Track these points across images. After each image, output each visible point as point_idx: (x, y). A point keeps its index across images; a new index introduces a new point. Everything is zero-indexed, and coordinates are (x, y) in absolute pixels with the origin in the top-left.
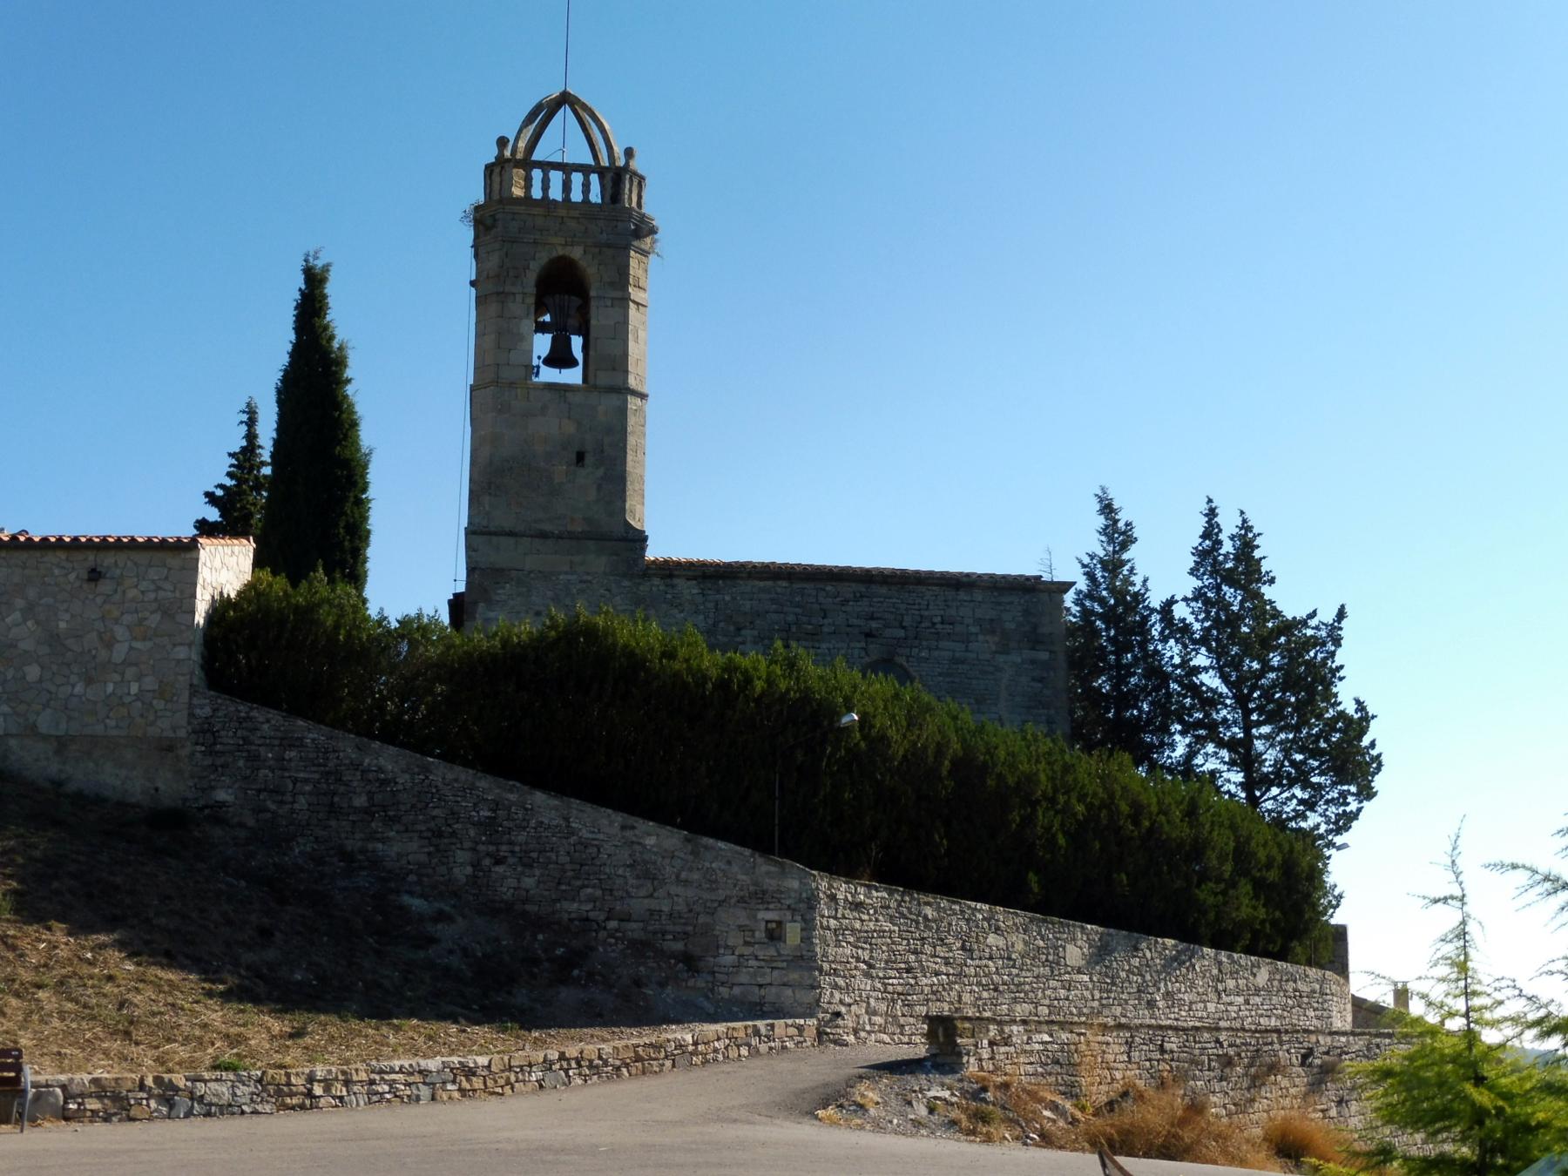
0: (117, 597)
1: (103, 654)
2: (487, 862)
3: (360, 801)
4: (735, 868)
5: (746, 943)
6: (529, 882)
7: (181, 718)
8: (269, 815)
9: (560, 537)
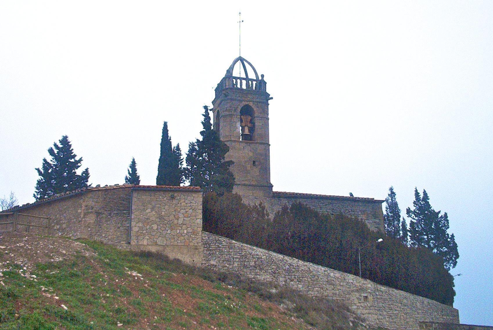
0: (179, 205)
1: (176, 221)
2: (288, 280)
3: (253, 264)
4: (355, 282)
5: (359, 303)
6: (300, 286)
7: (199, 240)
8: (226, 268)
9: (250, 185)
